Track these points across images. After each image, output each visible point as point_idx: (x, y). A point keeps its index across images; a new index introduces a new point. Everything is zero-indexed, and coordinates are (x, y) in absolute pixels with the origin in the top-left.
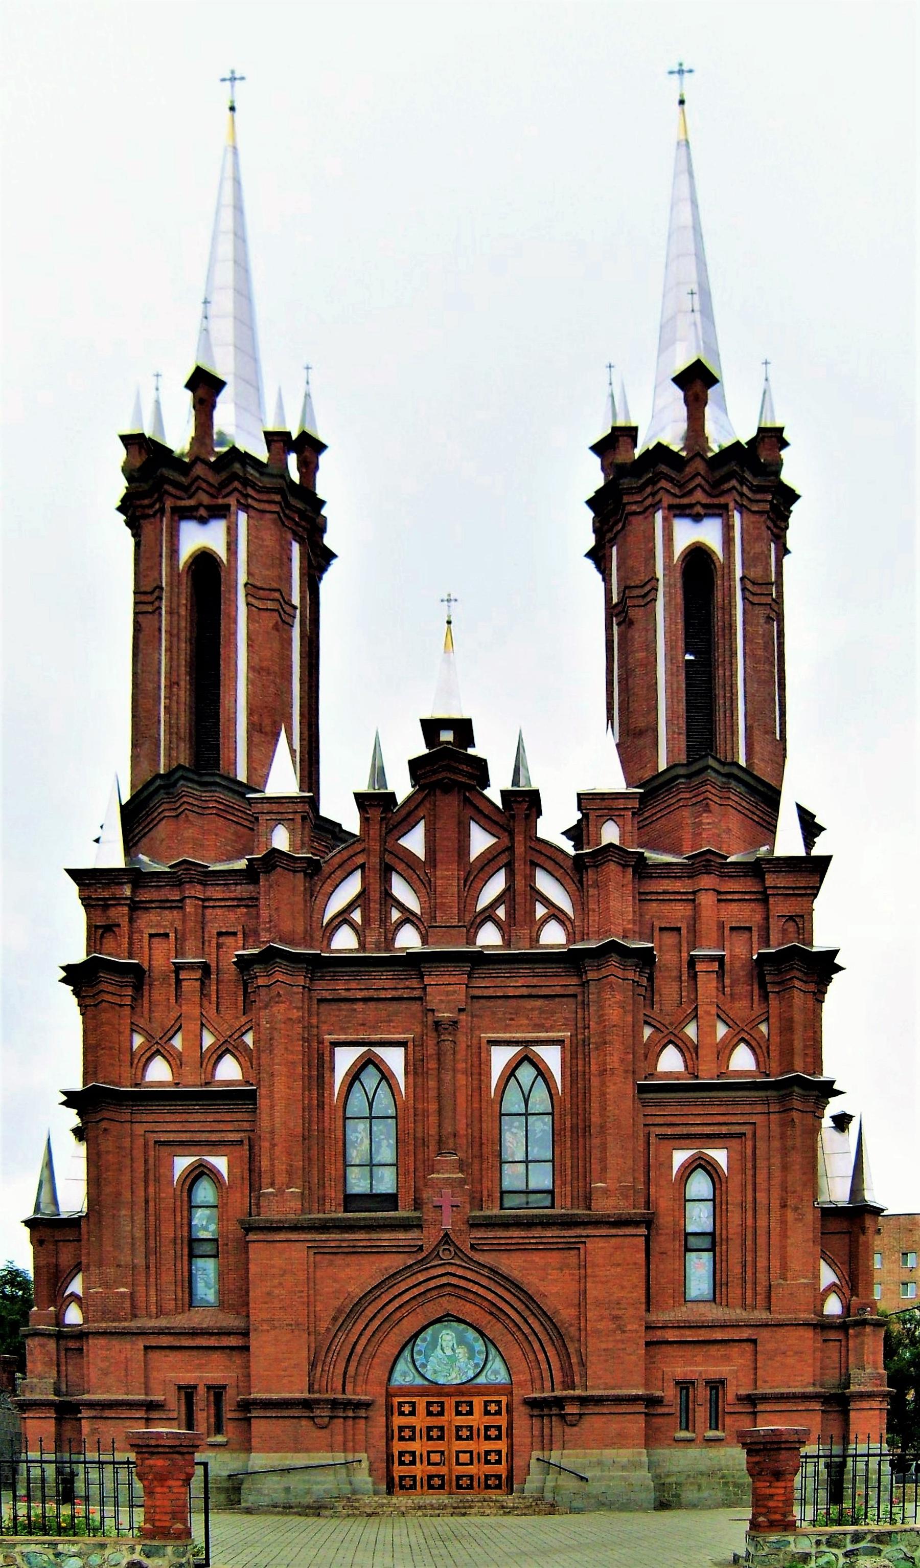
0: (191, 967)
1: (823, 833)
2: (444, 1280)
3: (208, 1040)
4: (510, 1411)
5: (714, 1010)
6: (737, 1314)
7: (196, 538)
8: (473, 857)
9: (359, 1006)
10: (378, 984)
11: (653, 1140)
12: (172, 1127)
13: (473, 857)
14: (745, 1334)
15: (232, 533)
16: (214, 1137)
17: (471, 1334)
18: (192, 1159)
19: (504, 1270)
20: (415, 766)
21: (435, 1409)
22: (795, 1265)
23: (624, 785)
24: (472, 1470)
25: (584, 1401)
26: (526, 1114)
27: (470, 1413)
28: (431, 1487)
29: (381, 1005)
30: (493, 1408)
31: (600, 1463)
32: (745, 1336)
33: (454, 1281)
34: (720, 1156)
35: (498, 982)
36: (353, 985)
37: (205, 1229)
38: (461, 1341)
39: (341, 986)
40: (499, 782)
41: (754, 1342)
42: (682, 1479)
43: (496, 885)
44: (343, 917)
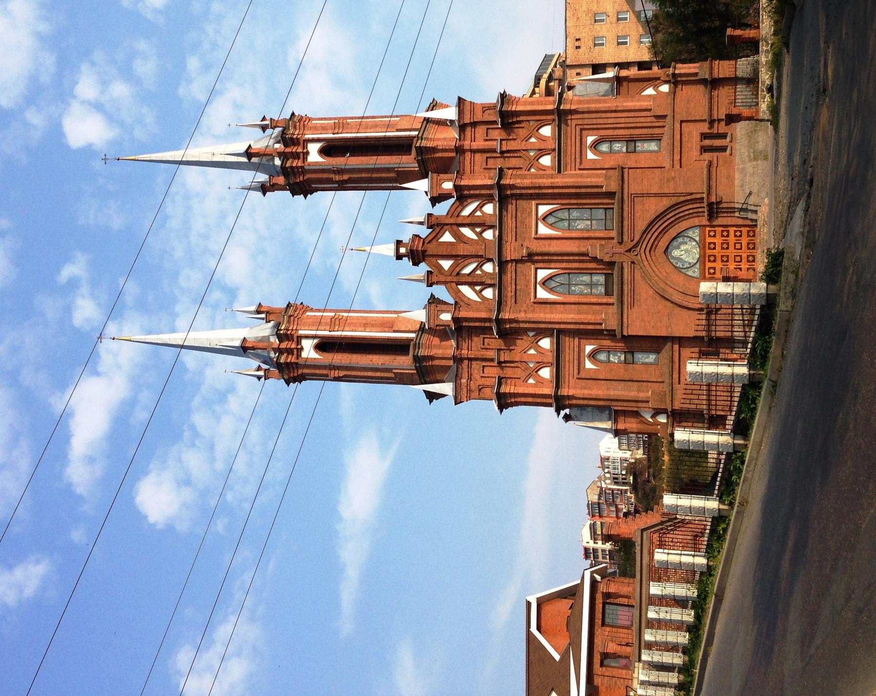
0: (499, 355)
1: (468, 98)
2: (647, 253)
3: (532, 352)
4: (714, 226)
5: (524, 142)
6: (667, 131)
7: (308, 350)
8: (454, 240)
9: (518, 287)
10: (509, 279)
11: (582, 167)
12: (571, 368)
13: (454, 240)
14: (677, 125)
15: (307, 337)
16: (576, 350)
17: (675, 243)
18: (587, 360)
19: (644, 228)
20: (416, 264)
21: (712, 259)
22: (645, 104)
23: (426, 180)
24: (744, 243)
25: (709, 194)
26: (569, 220)
27: (714, 244)
28: (753, 261)
29: (518, 278)
30: (712, 234)
31: (742, 186)
32: (679, 126)
33: (648, 249)
34: (590, 139)
35: (509, 231)
36: (509, 289)
37: (619, 357)
38: (678, 247)
39: (509, 294)
40: (424, 232)
41: (682, 122)
42: (752, 150)
43: (466, 232)
44: (479, 293)
